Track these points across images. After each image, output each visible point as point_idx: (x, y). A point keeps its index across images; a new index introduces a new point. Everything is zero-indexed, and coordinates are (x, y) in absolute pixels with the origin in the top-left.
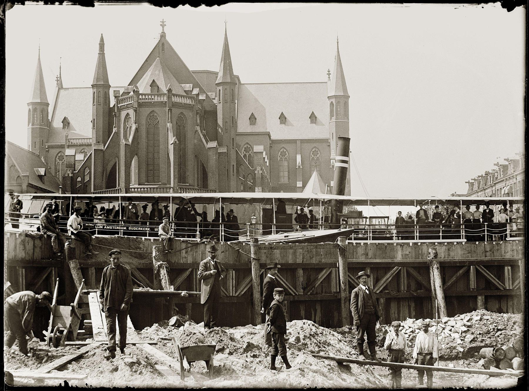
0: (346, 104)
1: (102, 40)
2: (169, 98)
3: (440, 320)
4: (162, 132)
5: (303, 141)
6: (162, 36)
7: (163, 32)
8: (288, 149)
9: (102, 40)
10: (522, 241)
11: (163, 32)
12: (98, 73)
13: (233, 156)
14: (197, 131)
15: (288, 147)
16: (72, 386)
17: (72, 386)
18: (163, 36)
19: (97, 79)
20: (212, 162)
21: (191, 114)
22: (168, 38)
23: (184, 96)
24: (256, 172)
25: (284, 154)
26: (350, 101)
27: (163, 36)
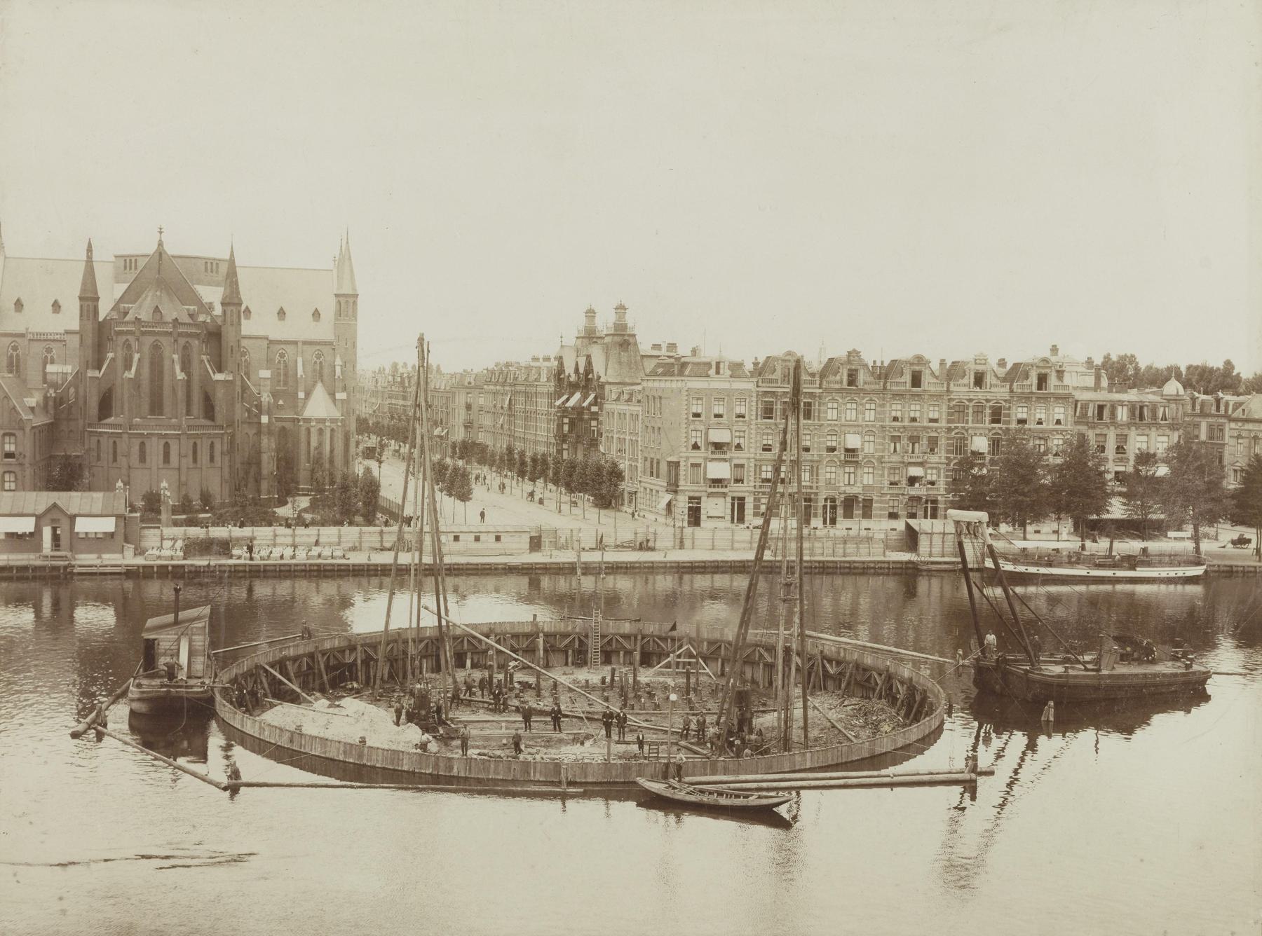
0: (355, 303)
1: (90, 245)
2: (174, 327)
3: (359, 647)
4: (167, 363)
6: (159, 245)
7: (160, 240)
8: (288, 351)
9: (90, 245)
10: (414, 625)
11: (160, 240)
12: (84, 284)
13: (239, 383)
14: (203, 361)
15: (290, 349)
16: (1239, 374)
17: (1239, 374)
18: (160, 244)
19: (83, 290)
20: (220, 395)
21: (197, 342)
22: (166, 248)
23: (189, 324)
24: (262, 399)
25: (282, 356)
27: (160, 244)
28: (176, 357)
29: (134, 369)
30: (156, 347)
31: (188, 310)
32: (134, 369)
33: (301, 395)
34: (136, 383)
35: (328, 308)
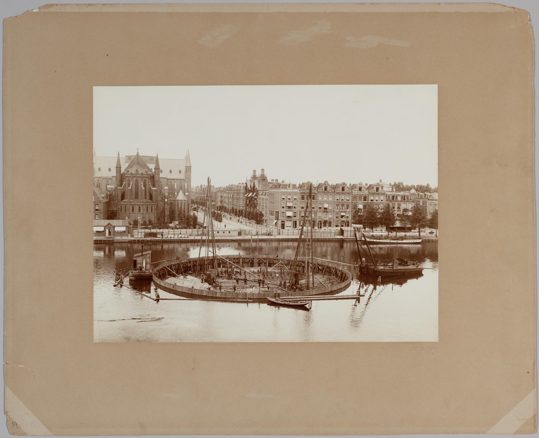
5: (177, 179)
15: (173, 181)
18: (138, 153)
26: (192, 168)
27: (138, 153)
28: (142, 183)
29: (131, 187)
30: (137, 181)
31: (145, 170)
32: (131, 187)
33: (176, 193)
34: (131, 190)
35: (183, 171)
